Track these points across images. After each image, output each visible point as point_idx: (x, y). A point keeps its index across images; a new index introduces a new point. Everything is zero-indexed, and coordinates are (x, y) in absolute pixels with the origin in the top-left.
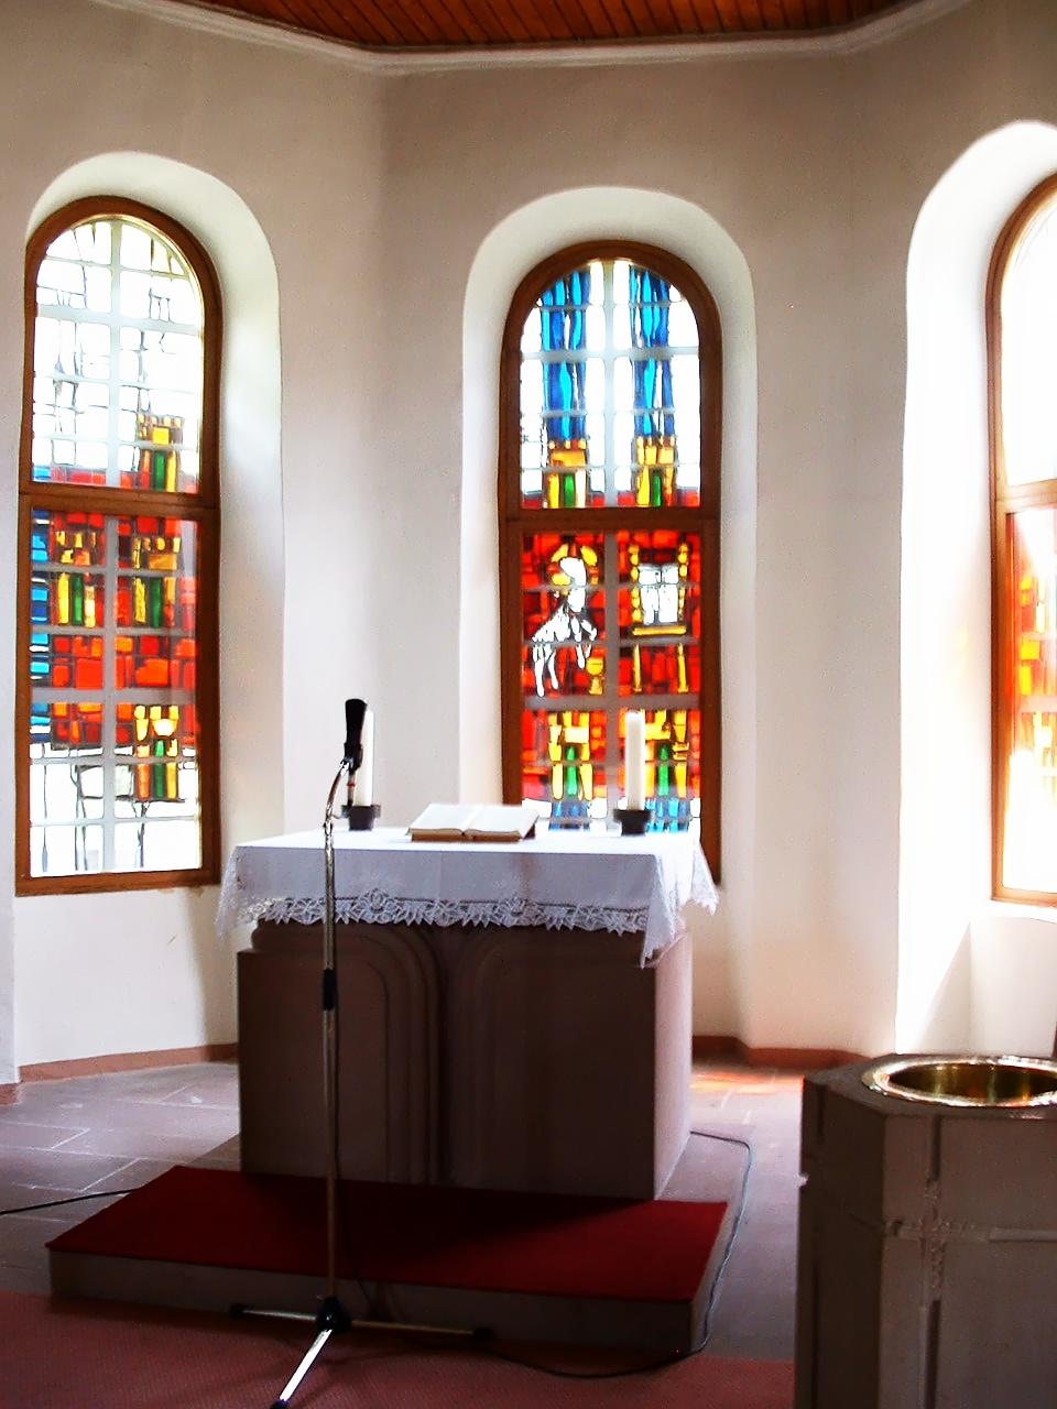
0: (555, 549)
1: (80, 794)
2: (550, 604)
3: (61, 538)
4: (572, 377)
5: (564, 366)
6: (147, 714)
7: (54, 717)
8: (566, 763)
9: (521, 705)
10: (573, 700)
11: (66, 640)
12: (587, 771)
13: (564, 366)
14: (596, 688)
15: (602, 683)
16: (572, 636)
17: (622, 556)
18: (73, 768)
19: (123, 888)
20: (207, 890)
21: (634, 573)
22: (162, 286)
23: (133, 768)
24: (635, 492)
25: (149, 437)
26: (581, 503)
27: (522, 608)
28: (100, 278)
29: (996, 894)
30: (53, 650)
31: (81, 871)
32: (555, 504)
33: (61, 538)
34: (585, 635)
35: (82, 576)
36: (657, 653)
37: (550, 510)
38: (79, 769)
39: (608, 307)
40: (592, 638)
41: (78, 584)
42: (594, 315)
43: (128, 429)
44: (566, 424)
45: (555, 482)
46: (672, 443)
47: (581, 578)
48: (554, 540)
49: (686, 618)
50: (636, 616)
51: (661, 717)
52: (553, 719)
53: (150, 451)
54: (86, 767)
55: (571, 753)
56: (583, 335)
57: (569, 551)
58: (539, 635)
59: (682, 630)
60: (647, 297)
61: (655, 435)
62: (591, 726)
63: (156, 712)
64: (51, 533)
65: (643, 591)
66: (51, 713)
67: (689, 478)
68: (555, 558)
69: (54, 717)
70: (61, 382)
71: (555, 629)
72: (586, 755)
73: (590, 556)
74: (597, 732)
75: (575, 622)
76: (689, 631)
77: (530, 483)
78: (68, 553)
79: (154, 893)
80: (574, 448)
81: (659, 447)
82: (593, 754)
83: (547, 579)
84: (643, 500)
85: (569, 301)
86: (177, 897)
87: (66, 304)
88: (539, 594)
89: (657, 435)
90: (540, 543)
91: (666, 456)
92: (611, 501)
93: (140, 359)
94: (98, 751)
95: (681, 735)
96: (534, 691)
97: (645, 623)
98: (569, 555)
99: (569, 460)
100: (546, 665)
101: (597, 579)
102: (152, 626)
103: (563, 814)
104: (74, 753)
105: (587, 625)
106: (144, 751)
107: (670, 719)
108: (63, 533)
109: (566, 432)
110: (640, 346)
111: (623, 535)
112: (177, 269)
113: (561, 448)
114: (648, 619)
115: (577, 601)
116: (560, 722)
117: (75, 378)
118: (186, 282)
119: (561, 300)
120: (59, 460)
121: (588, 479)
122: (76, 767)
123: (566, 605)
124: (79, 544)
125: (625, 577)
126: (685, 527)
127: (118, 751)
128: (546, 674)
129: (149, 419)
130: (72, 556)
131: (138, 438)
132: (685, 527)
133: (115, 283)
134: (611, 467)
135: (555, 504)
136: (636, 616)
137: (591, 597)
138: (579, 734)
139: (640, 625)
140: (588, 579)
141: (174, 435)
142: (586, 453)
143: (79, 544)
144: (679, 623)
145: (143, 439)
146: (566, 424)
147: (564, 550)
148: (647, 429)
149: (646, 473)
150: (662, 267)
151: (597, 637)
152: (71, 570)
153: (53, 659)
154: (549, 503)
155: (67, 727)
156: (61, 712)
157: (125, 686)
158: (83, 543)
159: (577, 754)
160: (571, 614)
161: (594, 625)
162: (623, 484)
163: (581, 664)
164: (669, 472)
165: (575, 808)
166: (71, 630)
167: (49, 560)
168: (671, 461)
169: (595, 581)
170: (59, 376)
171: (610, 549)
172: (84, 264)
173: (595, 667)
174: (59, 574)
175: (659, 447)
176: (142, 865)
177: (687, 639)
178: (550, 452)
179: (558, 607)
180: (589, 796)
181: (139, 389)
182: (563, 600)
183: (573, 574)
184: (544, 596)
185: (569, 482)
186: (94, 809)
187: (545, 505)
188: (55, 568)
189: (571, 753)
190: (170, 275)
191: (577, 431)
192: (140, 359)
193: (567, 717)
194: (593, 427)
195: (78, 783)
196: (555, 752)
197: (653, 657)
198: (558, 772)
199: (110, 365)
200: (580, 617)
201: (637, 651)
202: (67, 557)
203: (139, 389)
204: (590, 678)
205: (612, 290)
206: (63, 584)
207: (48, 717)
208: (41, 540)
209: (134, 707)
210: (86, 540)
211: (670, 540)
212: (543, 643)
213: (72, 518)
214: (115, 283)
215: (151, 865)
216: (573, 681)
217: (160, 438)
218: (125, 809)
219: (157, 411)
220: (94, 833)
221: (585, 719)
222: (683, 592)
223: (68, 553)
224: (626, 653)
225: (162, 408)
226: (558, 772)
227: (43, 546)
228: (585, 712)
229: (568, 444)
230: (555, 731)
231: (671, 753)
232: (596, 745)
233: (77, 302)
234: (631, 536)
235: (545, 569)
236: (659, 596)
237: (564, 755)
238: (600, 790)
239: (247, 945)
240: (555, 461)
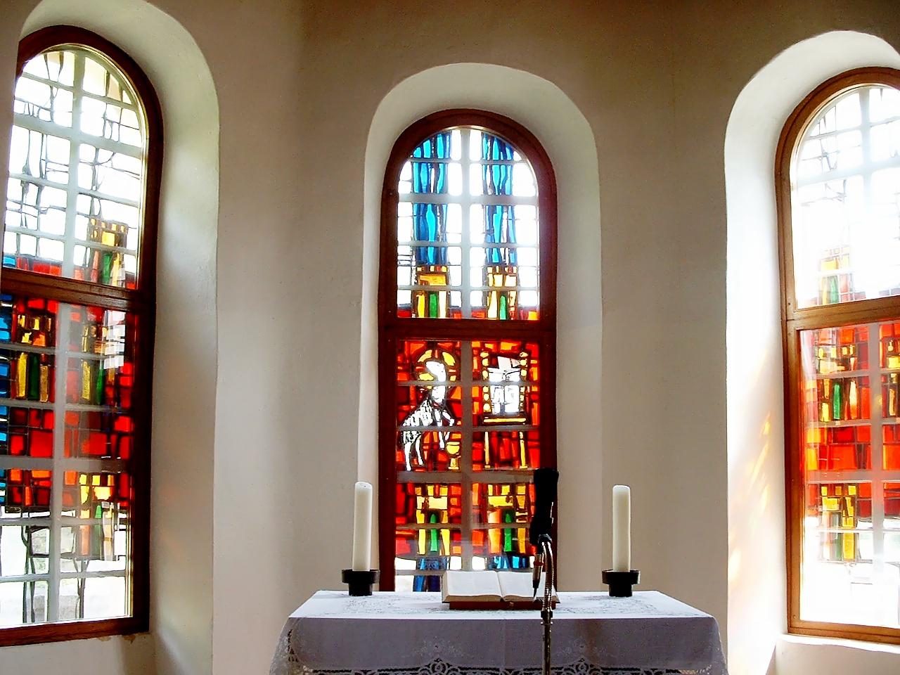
0: (422, 352)
1: (30, 553)
2: (417, 397)
3: (22, 321)
4: (436, 219)
5: (429, 206)
6: (89, 481)
7: (10, 482)
8: (429, 527)
9: (394, 477)
10: (434, 476)
11: (23, 413)
12: (446, 534)
13: (429, 206)
14: (453, 465)
15: (459, 462)
16: (434, 423)
17: (475, 361)
18: (25, 527)
19: (68, 637)
20: (139, 638)
21: (485, 374)
22: (113, 112)
23: (76, 530)
24: (485, 310)
25: (99, 239)
26: (443, 315)
27: (395, 400)
28: (65, 99)
29: (791, 629)
30: (12, 421)
31: (29, 624)
32: (421, 315)
33: (22, 321)
34: (446, 423)
35: (38, 356)
36: (502, 436)
37: (418, 320)
38: (30, 530)
39: (465, 162)
40: (451, 425)
41: (35, 361)
42: (453, 172)
43: (81, 229)
44: (431, 251)
45: (422, 299)
46: (515, 271)
47: (442, 377)
48: (417, 346)
49: (525, 411)
50: (486, 408)
51: (506, 490)
52: (418, 490)
53: (98, 250)
54: (36, 528)
55: (433, 520)
56: (445, 182)
57: (433, 354)
58: (408, 422)
59: (523, 420)
60: (496, 157)
61: (502, 265)
62: (449, 497)
63: (96, 480)
64: (14, 316)
65: (492, 388)
66: (6, 479)
67: (529, 300)
68: (422, 359)
69: (10, 482)
70: (28, 183)
71: (422, 416)
72: (445, 520)
73: (449, 359)
74: (454, 501)
75: (437, 413)
76: (529, 421)
77: (403, 298)
78: (27, 335)
79: (94, 641)
80: (436, 273)
81: (505, 274)
82: (451, 520)
83: (414, 377)
84: (492, 315)
85: (435, 155)
86: (113, 644)
87: (35, 115)
88: (408, 388)
89: (502, 267)
90: (409, 348)
91: (510, 281)
92: (467, 315)
93: (94, 171)
94: (47, 514)
95: (522, 505)
96: (404, 468)
97: (493, 413)
98: (432, 358)
99: (435, 281)
100: (413, 446)
101: (455, 377)
102: (95, 404)
103: (426, 568)
104: (25, 515)
105: (447, 416)
106: (85, 514)
107: (513, 492)
108: (24, 317)
109: (431, 259)
110: (490, 193)
111: (476, 344)
112: (126, 99)
113: (427, 272)
114: (496, 410)
115: (439, 395)
116: (425, 494)
117: (41, 181)
118: (133, 114)
119: (427, 155)
120: (22, 252)
121: (448, 297)
122: (27, 527)
123: (430, 398)
124: (37, 327)
125: (478, 377)
126: (537, 338)
127: (63, 513)
128: (413, 454)
129: (100, 224)
130: (31, 338)
131: (90, 239)
132: (537, 338)
133: (76, 103)
134: (466, 287)
135: (421, 315)
136: (486, 408)
137: (450, 392)
138: (439, 504)
139: (490, 415)
140: (448, 378)
141: (120, 240)
142: (446, 275)
143: (37, 327)
144: (521, 415)
145: (94, 240)
146: (431, 251)
147: (428, 354)
148: (495, 260)
149: (494, 294)
150: (510, 132)
151: (455, 424)
152: (30, 349)
153: (11, 429)
154: (417, 315)
155: (21, 491)
156: (15, 477)
157: (70, 456)
158: (40, 326)
159: (439, 520)
160: (433, 405)
161: (453, 416)
162: (476, 301)
163: (442, 445)
164: (513, 294)
165: (436, 563)
166: (28, 404)
167: (10, 340)
168: (514, 285)
169: (453, 378)
170: (26, 177)
171: (465, 355)
172: (53, 85)
173: (453, 449)
174: (19, 353)
175: (505, 274)
176: (33, 621)
177: (527, 427)
178: (418, 274)
179: (424, 399)
180: (447, 553)
181: (93, 197)
182: (427, 394)
183: (436, 373)
184: (412, 389)
185: (433, 297)
186: (42, 566)
187: (414, 316)
188: (15, 347)
189: (433, 520)
190: (120, 103)
191: (440, 259)
192: (94, 171)
193: (430, 489)
194: (453, 255)
195: (28, 543)
196: (420, 518)
197: (500, 441)
198: (422, 533)
199: (67, 174)
200: (440, 408)
201: (487, 434)
202: (26, 338)
203: (93, 197)
204: (449, 456)
205: (466, 148)
206: (22, 362)
207: (4, 482)
208: (5, 322)
209: (78, 475)
210: (42, 324)
211: (513, 347)
212: (410, 429)
213: (31, 304)
214: (76, 103)
215: (90, 616)
216: (435, 458)
217: (109, 240)
218: (67, 566)
219: (106, 216)
220: (41, 589)
221: (444, 491)
222: (523, 390)
223: (27, 335)
224: (479, 438)
225: (111, 213)
226: (422, 533)
227: (419, 149)
228: (445, 484)
229: (432, 269)
230: (420, 500)
231: (514, 518)
232: (453, 512)
233: (45, 116)
234: (483, 345)
235: (414, 368)
236: (505, 389)
237: (427, 520)
238: (457, 549)
239: (643, 669)
240: (422, 281)
